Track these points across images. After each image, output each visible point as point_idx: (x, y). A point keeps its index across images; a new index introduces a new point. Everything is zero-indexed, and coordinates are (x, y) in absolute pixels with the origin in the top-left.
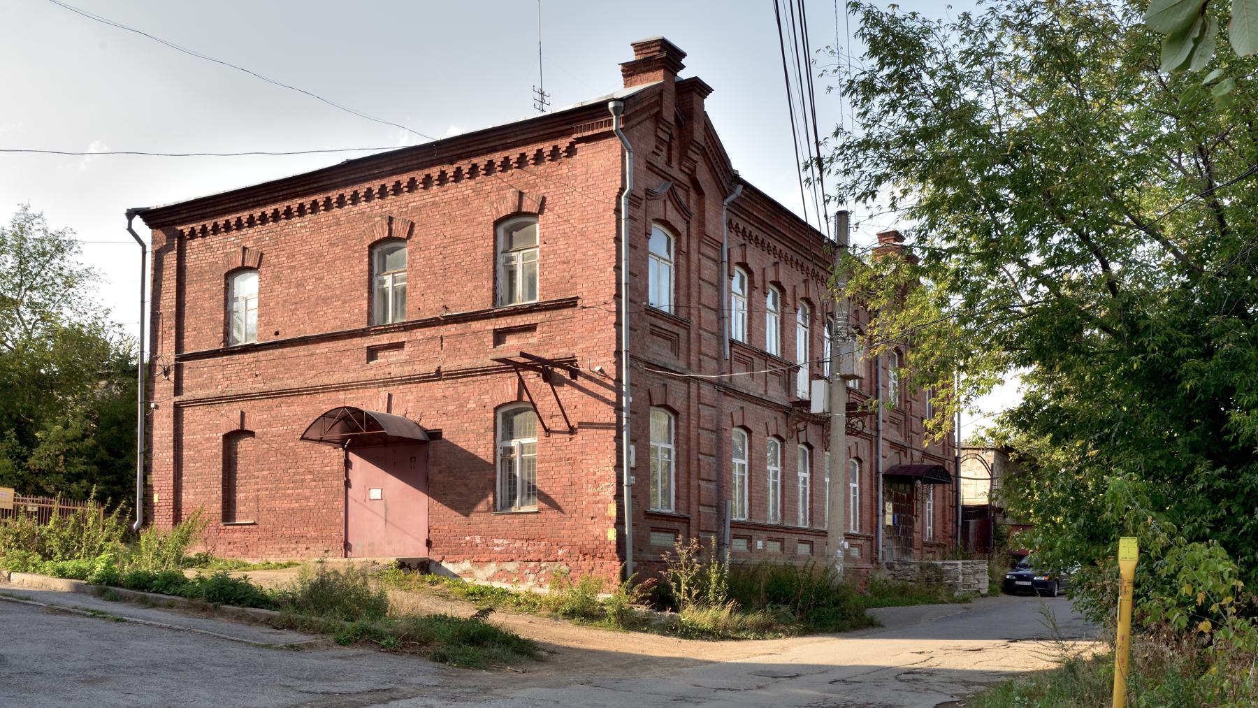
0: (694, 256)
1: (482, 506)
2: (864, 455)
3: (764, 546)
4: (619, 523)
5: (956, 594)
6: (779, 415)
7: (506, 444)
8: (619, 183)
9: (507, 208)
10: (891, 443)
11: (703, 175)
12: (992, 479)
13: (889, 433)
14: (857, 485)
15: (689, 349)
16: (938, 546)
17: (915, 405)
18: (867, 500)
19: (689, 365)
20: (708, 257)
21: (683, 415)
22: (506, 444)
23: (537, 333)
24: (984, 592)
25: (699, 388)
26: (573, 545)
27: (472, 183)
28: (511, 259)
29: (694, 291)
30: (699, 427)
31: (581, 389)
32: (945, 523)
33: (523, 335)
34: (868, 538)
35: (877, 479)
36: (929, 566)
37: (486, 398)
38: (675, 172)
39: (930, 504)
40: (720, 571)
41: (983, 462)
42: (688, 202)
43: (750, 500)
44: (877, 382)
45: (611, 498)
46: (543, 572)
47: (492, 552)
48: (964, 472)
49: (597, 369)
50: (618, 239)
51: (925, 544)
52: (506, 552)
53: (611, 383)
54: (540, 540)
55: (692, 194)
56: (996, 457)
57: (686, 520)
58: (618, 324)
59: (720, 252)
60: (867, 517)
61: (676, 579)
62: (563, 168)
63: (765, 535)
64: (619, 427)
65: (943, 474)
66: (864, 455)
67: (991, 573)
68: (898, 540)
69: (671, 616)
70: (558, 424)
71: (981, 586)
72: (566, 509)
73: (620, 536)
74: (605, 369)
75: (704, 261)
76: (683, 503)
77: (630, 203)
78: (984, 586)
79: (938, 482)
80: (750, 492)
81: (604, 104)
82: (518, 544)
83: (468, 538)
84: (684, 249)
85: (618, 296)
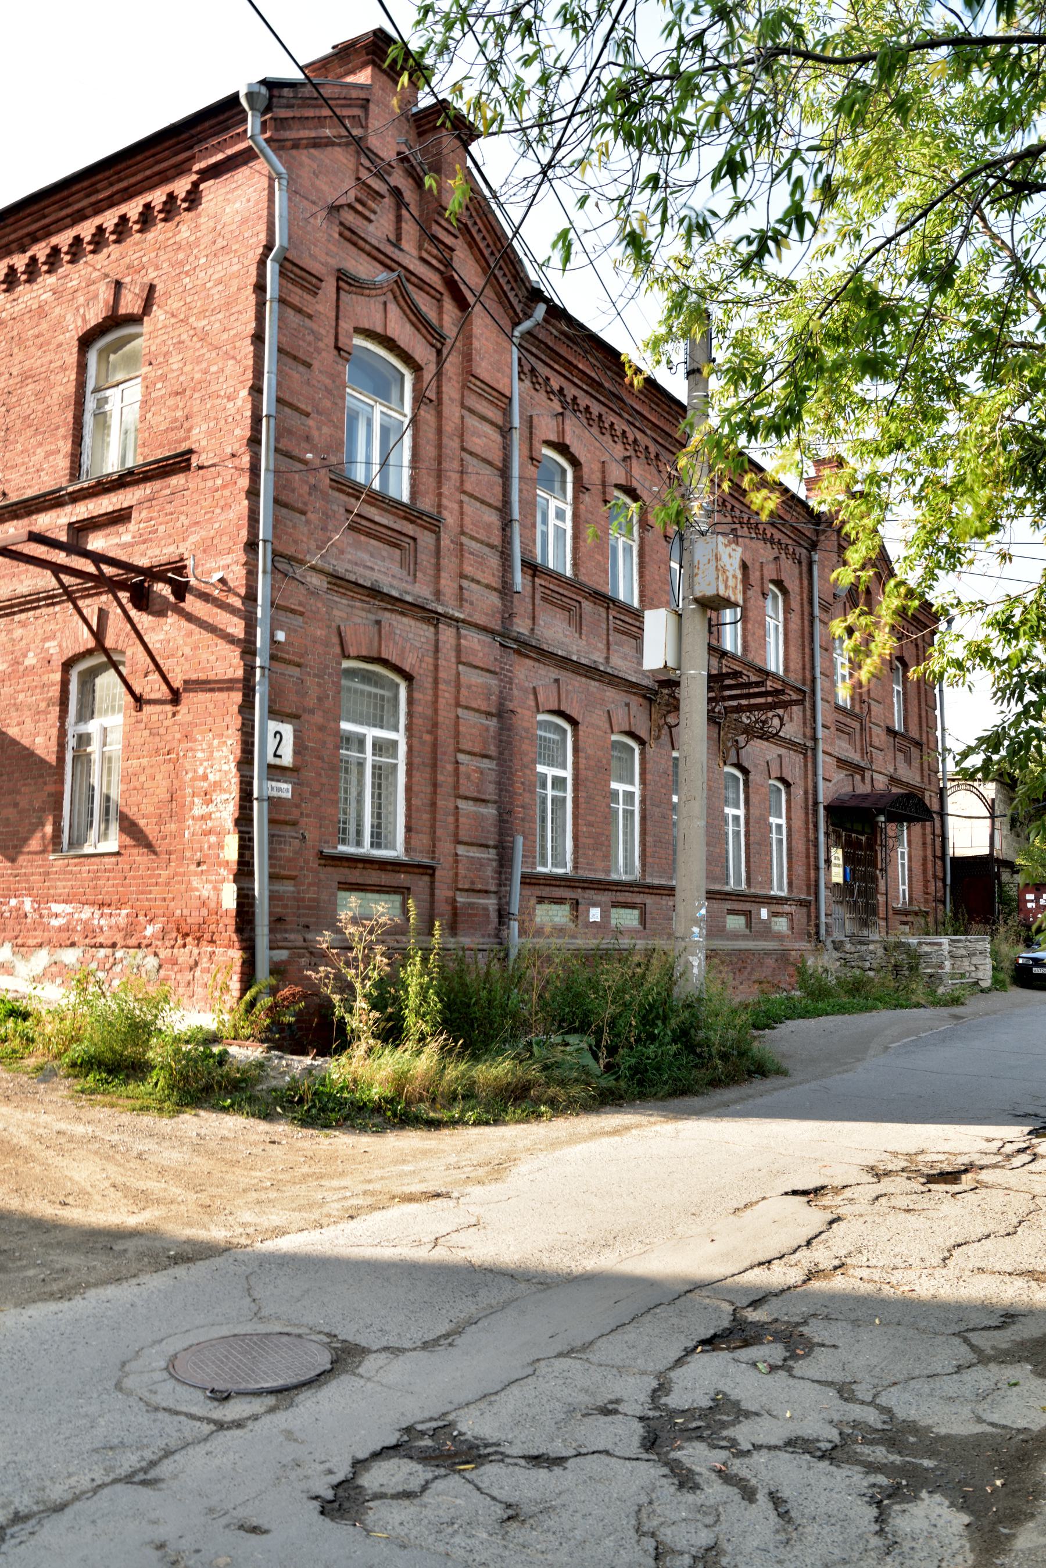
0: (452, 411)
1: (34, 844)
2: (794, 774)
3: (605, 915)
4: (244, 870)
5: (941, 990)
6: (635, 701)
7: (83, 728)
8: (263, 237)
9: (95, 316)
10: (839, 760)
11: (468, 271)
12: (993, 817)
13: (833, 745)
14: (783, 821)
15: (438, 568)
16: (916, 914)
17: (876, 708)
18: (800, 846)
19: (438, 593)
20: (483, 418)
21: (424, 681)
22: (83, 728)
23: (132, 526)
24: (986, 984)
25: (459, 636)
26: (169, 916)
27: (51, 280)
28: (106, 400)
29: (451, 466)
30: (458, 705)
31: (190, 618)
32: (926, 881)
33: (112, 529)
34: (801, 903)
35: (816, 812)
36: (899, 945)
37: (52, 646)
38: (410, 256)
39: (902, 854)
40: (425, 971)
41: (981, 797)
42: (441, 320)
43: (576, 838)
44: (813, 668)
45: (230, 825)
46: (118, 969)
47: (46, 928)
48: (951, 807)
49: (216, 577)
50: (258, 338)
51: (897, 912)
52: (66, 929)
53: (237, 603)
54: (121, 904)
55: (448, 305)
56: (997, 791)
57: (429, 871)
58: (253, 493)
59: (507, 413)
60: (800, 870)
61: (347, 988)
62: (185, 228)
63: (606, 897)
64: (248, 688)
65: (920, 809)
66: (794, 774)
67: (995, 955)
68: (854, 907)
69: (309, 1071)
70: (152, 687)
71: (980, 975)
72: (160, 846)
73: (245, 900)
74: (229, 577)
75: (472, 421)
76: (422, 840)
77: (282, 274)
78: (985, 975)
79: (918, 820)
80: (575, 825)
81: (234, 98)
82: (86, 913)
83: (13, 902)
84: (431, 394)
85: (254, 441)
